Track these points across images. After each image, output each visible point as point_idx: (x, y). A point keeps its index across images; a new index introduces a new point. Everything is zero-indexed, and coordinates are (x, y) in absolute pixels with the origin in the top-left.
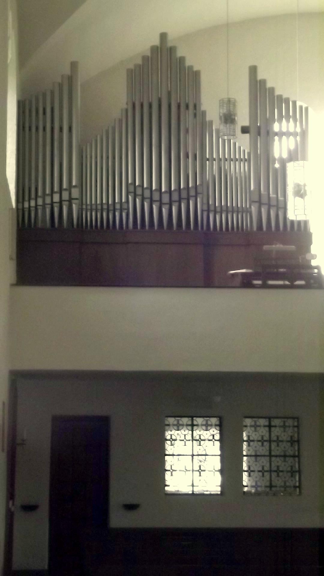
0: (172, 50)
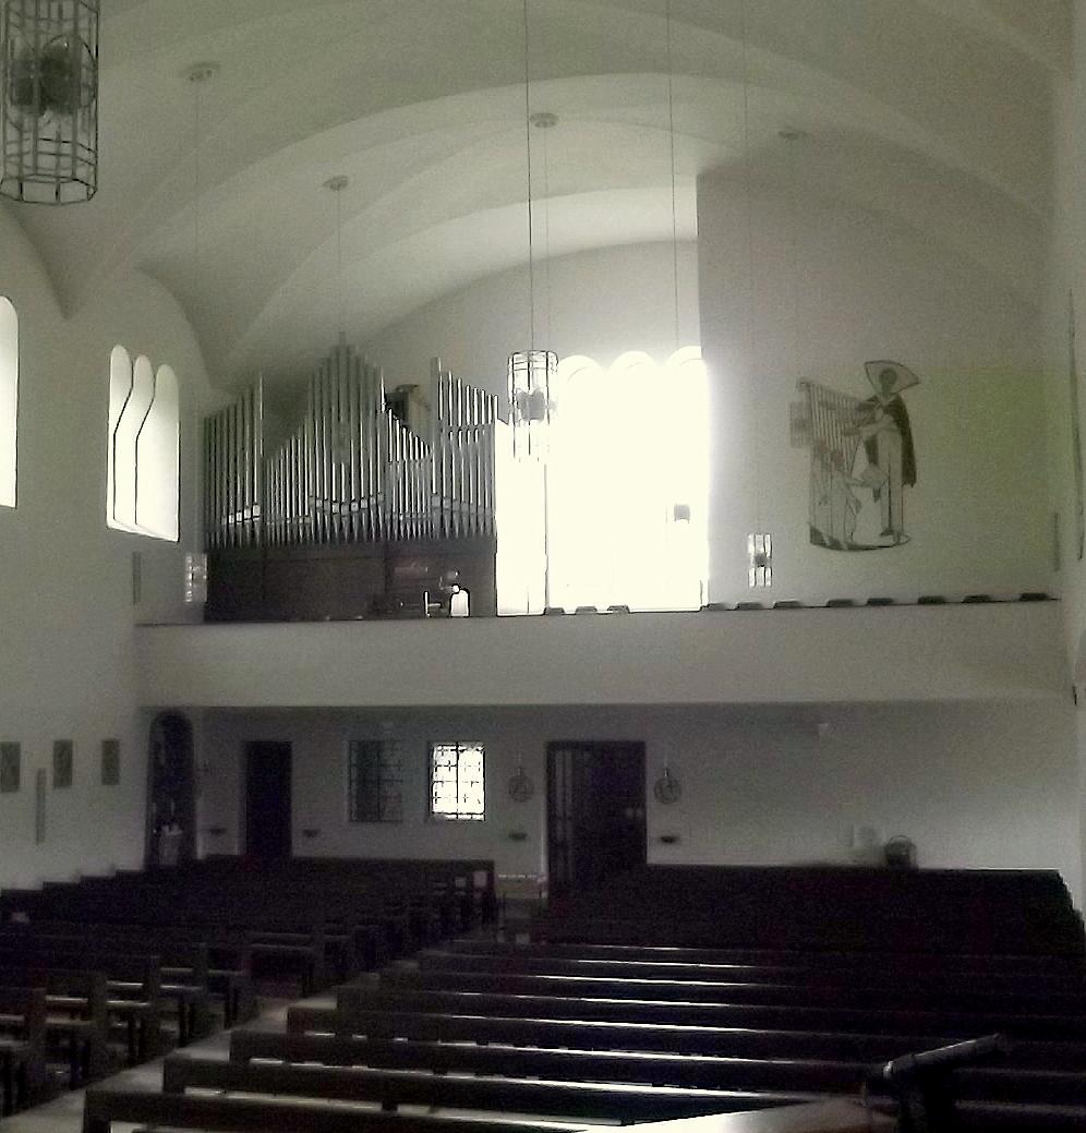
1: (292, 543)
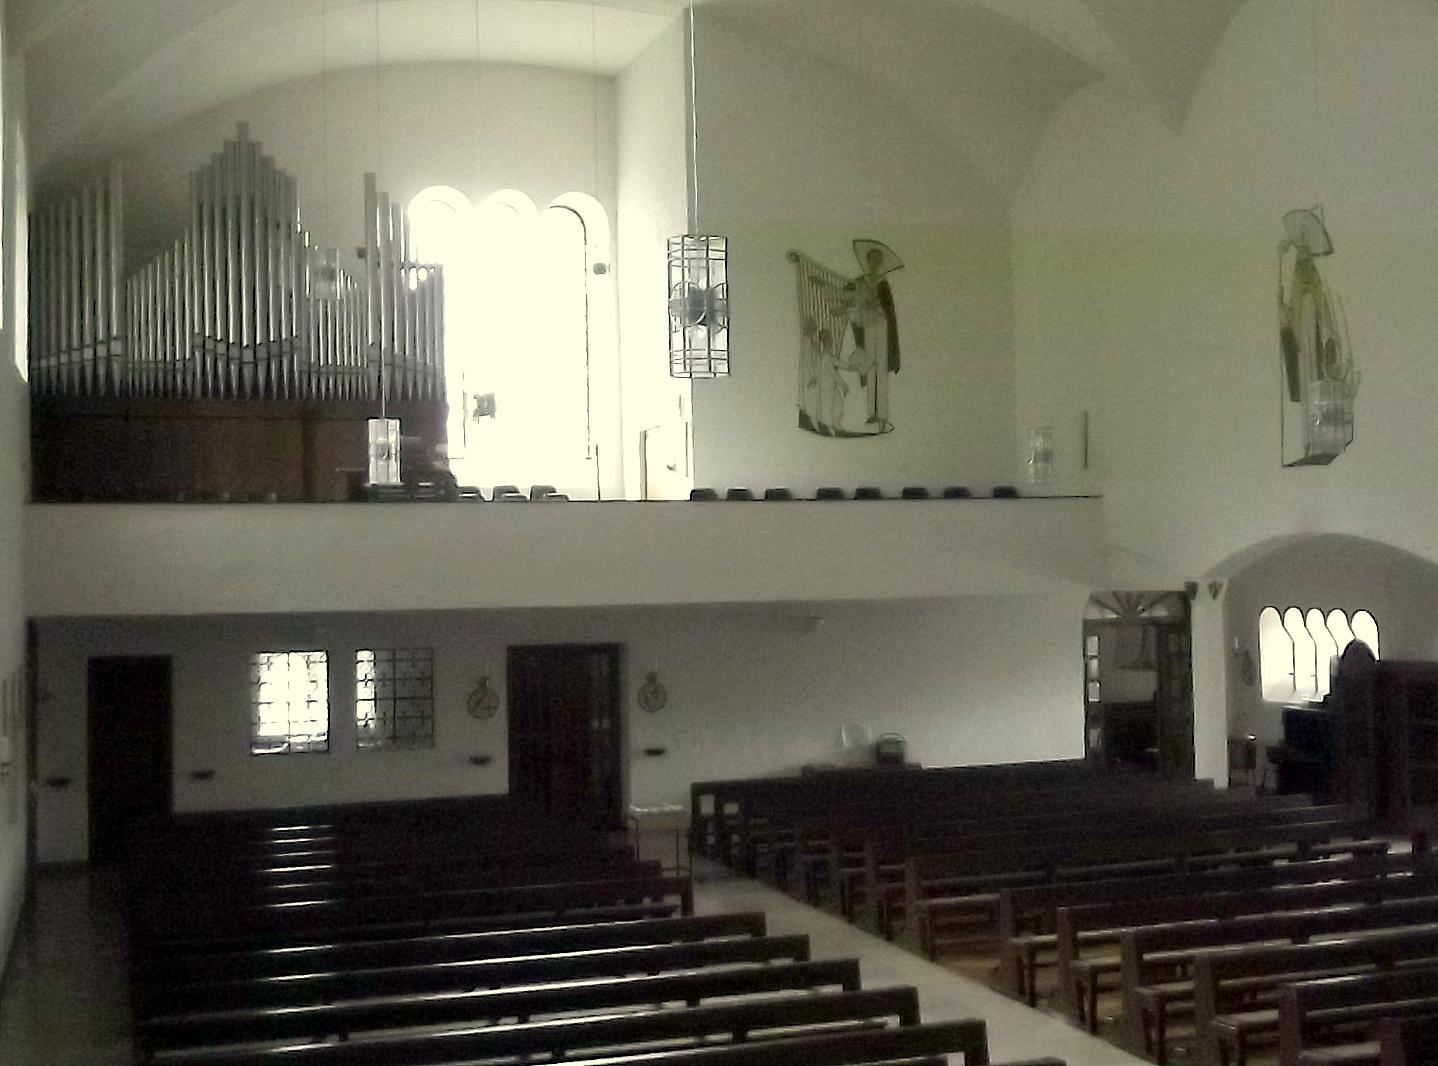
0: (253, 147)
1: (166, 393)
